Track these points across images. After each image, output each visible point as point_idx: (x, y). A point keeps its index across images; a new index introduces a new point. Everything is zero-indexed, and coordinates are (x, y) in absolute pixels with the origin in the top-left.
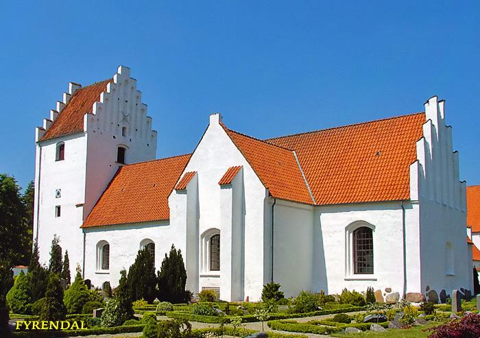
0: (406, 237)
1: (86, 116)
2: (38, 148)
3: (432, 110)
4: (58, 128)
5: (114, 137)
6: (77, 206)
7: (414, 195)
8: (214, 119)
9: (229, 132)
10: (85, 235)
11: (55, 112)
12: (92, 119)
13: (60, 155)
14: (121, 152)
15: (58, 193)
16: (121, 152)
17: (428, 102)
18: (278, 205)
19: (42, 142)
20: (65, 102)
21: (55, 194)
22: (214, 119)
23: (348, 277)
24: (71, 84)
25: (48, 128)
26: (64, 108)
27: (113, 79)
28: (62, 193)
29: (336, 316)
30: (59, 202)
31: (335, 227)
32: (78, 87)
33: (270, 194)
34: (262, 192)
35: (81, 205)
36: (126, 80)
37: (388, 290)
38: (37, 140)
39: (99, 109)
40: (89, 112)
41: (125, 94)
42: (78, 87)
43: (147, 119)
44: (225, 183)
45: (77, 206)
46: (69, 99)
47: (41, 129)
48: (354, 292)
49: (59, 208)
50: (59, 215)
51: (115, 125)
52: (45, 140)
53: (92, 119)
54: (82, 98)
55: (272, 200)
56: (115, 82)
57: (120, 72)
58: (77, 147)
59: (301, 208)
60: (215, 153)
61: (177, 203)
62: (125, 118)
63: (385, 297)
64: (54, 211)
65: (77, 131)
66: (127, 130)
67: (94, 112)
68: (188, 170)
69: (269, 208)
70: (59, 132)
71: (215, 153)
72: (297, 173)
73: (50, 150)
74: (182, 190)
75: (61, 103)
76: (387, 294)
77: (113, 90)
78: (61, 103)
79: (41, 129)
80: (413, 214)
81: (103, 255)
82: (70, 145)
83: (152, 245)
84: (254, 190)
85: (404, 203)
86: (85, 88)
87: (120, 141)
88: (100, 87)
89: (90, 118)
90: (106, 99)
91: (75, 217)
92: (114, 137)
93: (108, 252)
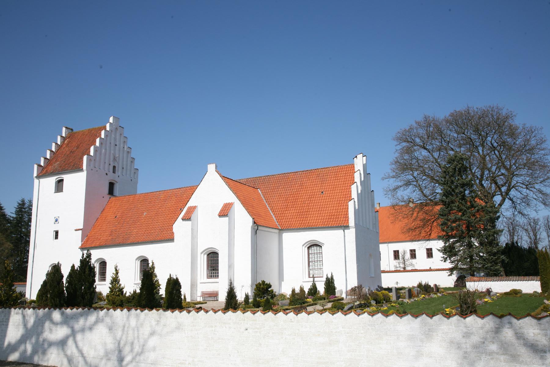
2: (36, 181)
3: (359, 162)
6: (76, 230)
7: (352, 222)
8: (211, 168)
9: (223, 177)
14: (111, 185)
15: (56, 221)
16: (111, 185)
17: (356, 157)
19: (38, 177)
21: (54, 220)
22: (211, 168)
26: (59, 147)
28: (59, 220)
29: (92, 269)
32: (70, 131)
33: (255, 223)
34: (249, 220)
35: (81, 229)
36: (117, 128)
38: (35, 174)
39: (96, 151)
41: (115, 139)
43: (131, 160)
45: (76, 230)
47: (39, 166)
49: (57, 233)
51: (107, 165)
52: (44, 173)
55: (257, 226)
58: (76, 182)
60: (212, 191)
61: (180, 227)
62: (115, 159)
64: (53, 234)
66: (117, 169)
68: (190, 204)
69: (254, 233)
70: (60, 165)
71: (212, 191)
73: (51, 181)
74: (187, 218)
75: (56, 144)
78: (56, 144)
79: (39, 166)
80: (351, 233)
82: (69, 179)
83: (210, 276)
84: (243, 218)
87: (112, 177)
88: (95, 133)
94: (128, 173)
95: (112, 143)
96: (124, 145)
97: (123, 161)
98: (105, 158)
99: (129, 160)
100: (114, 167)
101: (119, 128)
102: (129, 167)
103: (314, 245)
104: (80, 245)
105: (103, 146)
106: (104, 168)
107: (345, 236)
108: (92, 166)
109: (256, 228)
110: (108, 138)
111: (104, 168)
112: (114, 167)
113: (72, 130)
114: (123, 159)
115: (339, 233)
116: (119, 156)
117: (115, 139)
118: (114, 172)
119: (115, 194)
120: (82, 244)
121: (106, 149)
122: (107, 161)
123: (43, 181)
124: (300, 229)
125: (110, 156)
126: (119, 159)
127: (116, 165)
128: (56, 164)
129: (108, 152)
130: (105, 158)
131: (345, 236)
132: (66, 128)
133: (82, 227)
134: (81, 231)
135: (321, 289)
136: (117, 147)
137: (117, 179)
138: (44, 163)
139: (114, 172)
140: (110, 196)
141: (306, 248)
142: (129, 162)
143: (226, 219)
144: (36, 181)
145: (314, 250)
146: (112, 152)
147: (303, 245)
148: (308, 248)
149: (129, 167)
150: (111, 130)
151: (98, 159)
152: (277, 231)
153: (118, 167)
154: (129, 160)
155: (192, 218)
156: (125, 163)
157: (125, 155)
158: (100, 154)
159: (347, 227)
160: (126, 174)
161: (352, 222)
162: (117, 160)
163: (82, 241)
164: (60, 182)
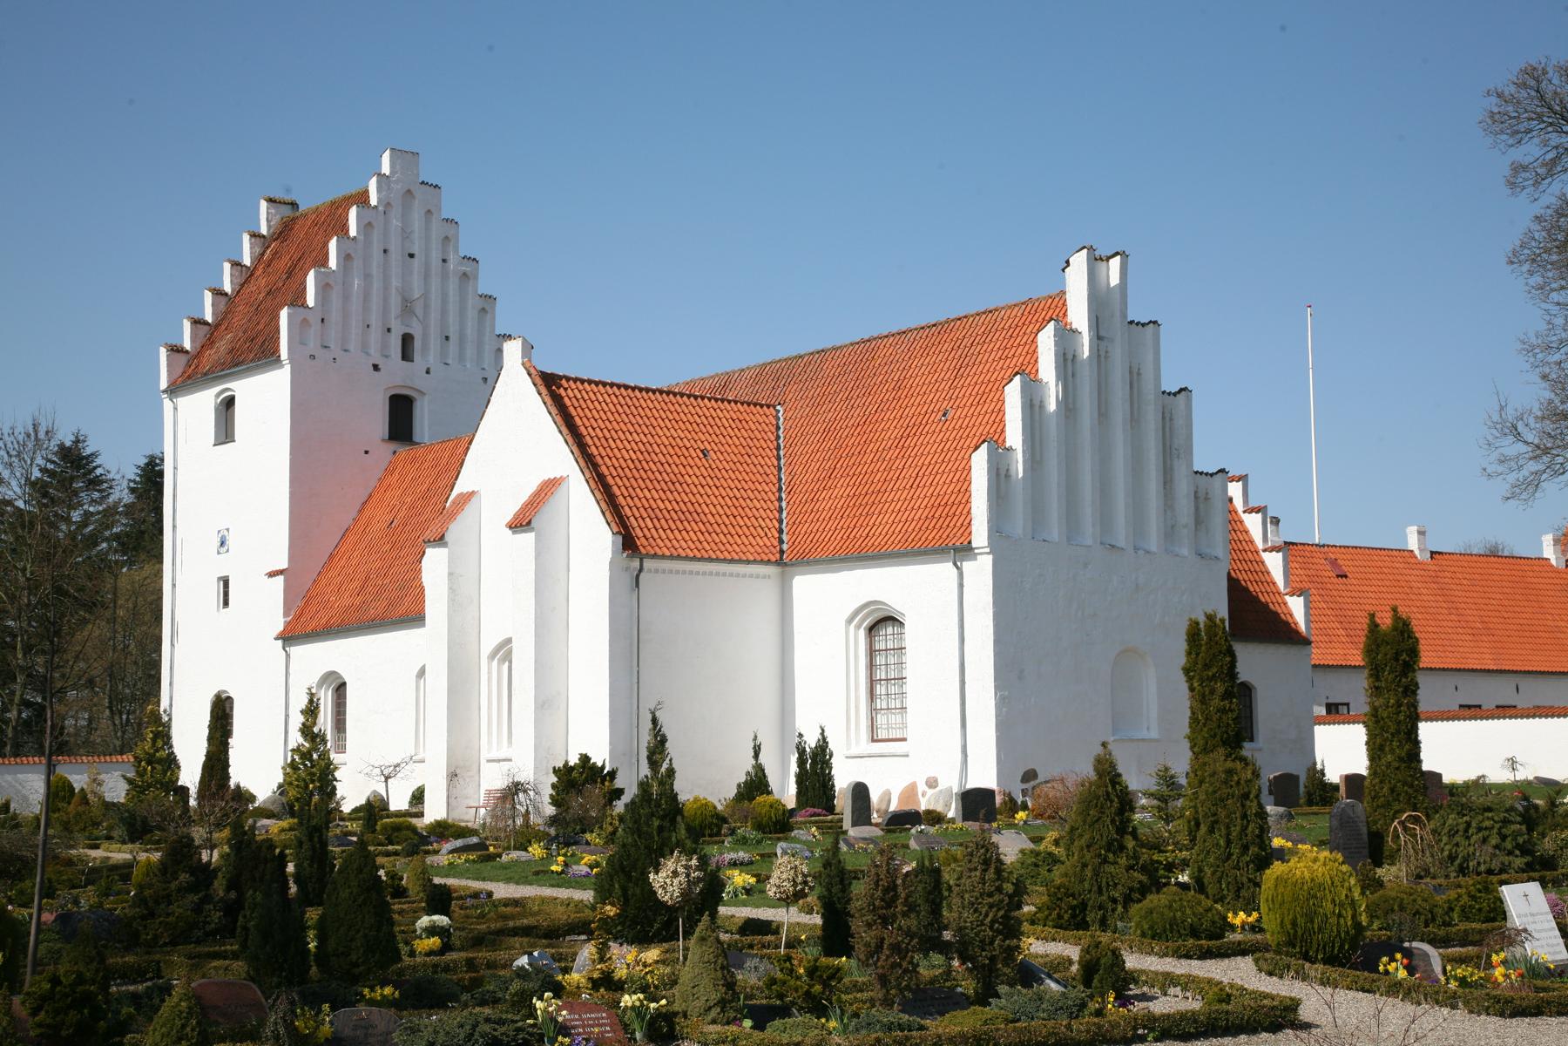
1: (284, 314)
2: (167, 404)
4: (222, 346)
5: (376, 367)
6: (272, 574)
7: (980, 534)
10: (288, 656)
11: (236, 264)
12: (305, 321)
13: (225, 431)
15: (222, 544)
18: (650, 571)
19: (175, 390)
20: (247, 261)
23: (854, 751)
24: (263, 205)
25: (198, 345)
26: (246, 276)
27: (366, 192)
32: (287, 211)
35: (281, 572)
36: (414, 190)
37: (932, 783)
38: (164, 384)
39: (324, 288)
40: (298, 300)
41: (406, 234)
42: (287, 211)
44: (521, 523)
45: (272, 574)
46: (258, 250)
47: (176, 350)
50: (226, 603)
51: (375, 335)
52: (191, 374)
53: (305, 321)
54: (296, 239)
56: (374, 201)
57: (386, 169)
58: (265, 396)
62: (407, 308)
64: (214, 590)
66: (417, 344)
67: (311, 301)
68: (461, 487)
69: (627, 580)
70: (228, 348)
72: (677, 485)
73: (200, 405)
76: (930, 792)
77: (366, 227)
80: (980, 570)
81: (1183, 1016)
86: (305, 215)
87: (398, 375)
90: (345, 258)
91: (265, 604)
92: (376, 367)
93: (449, 749)
94: (470, 352)
95: (392, 249)
96: (444, 251)
97: (444, 312)
98: (366, 308)
99: (470, 303)
100: (407, 340)
101: (419, 192)
102: (470, 330)
103: (882, 622)
104: (279, 626)
105: (357, 263)
106: (364, 348)
107: (961, 586)
108: (313, 345)
109: (636, 563)
110: (376, 235)
111: (364, 348)
112: (407, 340)
113: (294, 205)
114: (444, 301)
115: (941, 572)
116: (426, 296)
117: (406, 234)
118: (407, 355)
119: (416, 438)
120: (287, 624)
121: (367, 277)
122: (375, 320)
123: (184, 402)
124: (905, 555)
125: (386, 300)
126: (426, 307)
127: (417, 332)
128: (222, 346)
129: (376, 285)
130: (366, 308)
131: (961, 586)
132: (270, 200)
133: (285, 566)
134: (281, 579)
135: (786, 791)
136: (416, 261)
137: (421, 381)
138: (193, 340)
139: (407, 355)
140: (393, 446)
141: (862, 633)
142: (472, 314)
143: (528, 538)
144: (167, 404)
145: (887, 636)
146: (395, 283)
147: (850, 621)
148: (872, 629)
149: (470, 330)
150: (387, 205)
151: (334, 316)
152: (772, 570)
153: (425, 335)
154: (472, 304)
155: (448, 538)
156: (452, 318)
157: (453, 285)
158: (346, 297)
159: (964, 550)
160: (461, 358)
161: (980, 534)
162: (419, 311)
163: (286, 614)
164: (229, 403)
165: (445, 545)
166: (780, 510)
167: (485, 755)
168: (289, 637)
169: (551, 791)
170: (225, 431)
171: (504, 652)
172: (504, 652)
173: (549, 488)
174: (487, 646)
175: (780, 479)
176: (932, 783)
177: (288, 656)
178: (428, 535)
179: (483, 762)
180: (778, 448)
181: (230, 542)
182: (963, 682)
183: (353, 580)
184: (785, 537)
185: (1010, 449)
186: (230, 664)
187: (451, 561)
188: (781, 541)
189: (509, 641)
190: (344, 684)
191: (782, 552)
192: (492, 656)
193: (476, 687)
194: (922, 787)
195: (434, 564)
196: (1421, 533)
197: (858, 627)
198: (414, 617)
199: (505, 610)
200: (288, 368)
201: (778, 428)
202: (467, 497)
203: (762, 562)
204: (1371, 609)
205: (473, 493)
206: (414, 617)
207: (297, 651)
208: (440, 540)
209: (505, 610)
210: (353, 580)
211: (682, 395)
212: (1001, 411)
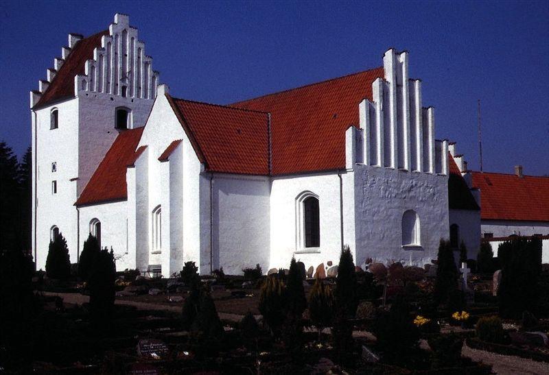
0: (37, 245)
1: (76, 78)
6: (72, 180)
10: (78, 211)
13: (55, 124)
19: (38, 107)
23: (299, 250)
27: (109, 30)
30: (55, 176)
31: (284, 195)
37: (330, 263)
38: (31, 107)
40: (82, 72)
44: (163, 158)
45: (72, 180)
46: (68, 53)
48: (61, 234)
50: (55, 192)
58: (69, 110)
59: (257, 180)
63: (326, 271)
65: (67, 94)
72: (235, 151)
73: (44, 115)
76: (329, 267)
80: (349, 178)
85: (340, 169)
87: (120, 102)
89: (81, 80)
91: (70, 192)
92: (112, 99)
104: (75, 200)
107: (341, 185)
115: (334, 178)
116: (131, 72)
123: (38, 112)
126: (132, 76)
131: (341, 185)
132: (72, 35)
133: (77, 176)
134: (75, 181)
143: (167, 164)
147: (297, 198)
152: (266, 179)
161: (349, 163)
163: (77, 196)
164: (55, 115)
165: (134, 167)
166: (269, 154)
167: (151, 251)
168: (79, 204)
169: (184, 265)
170: (55, 124)
171: (158, 210)
172: (158, 210)
173: (175, 145)
174: (151, 207)
175: (269, 142)
176: (330, 263)
177: (78, 211)
178: (128, 163)
179: (150, 254)
180: (268, 130)
181: (57, 167)
182: (342, 223)
183: (104, 184)
184: (271, 166)
185: (361, 129)
186: (57, 215)
187: (138, 175)
188: (269, 166)
189: (160, 206)
190: (100, 223)
191: (270, 171)
192: (153, 212)
193: (160, 221)
194: (326, 265)
195: (131, 174)
196: (520, 168)
197: (300, 201)
198: (123, 198)
199: (157, 193)
200: (78, 99)
201: (268, 122)
202: (143, 148)
203: (262, 175)
204: (162, 253)
205: (146, 146)
206: (123, 198)
207: (82, 210)
208: (133, 166)
209: (157, 193)
210: (104, 184)
211: (229, 108)
212: (358, 114)
